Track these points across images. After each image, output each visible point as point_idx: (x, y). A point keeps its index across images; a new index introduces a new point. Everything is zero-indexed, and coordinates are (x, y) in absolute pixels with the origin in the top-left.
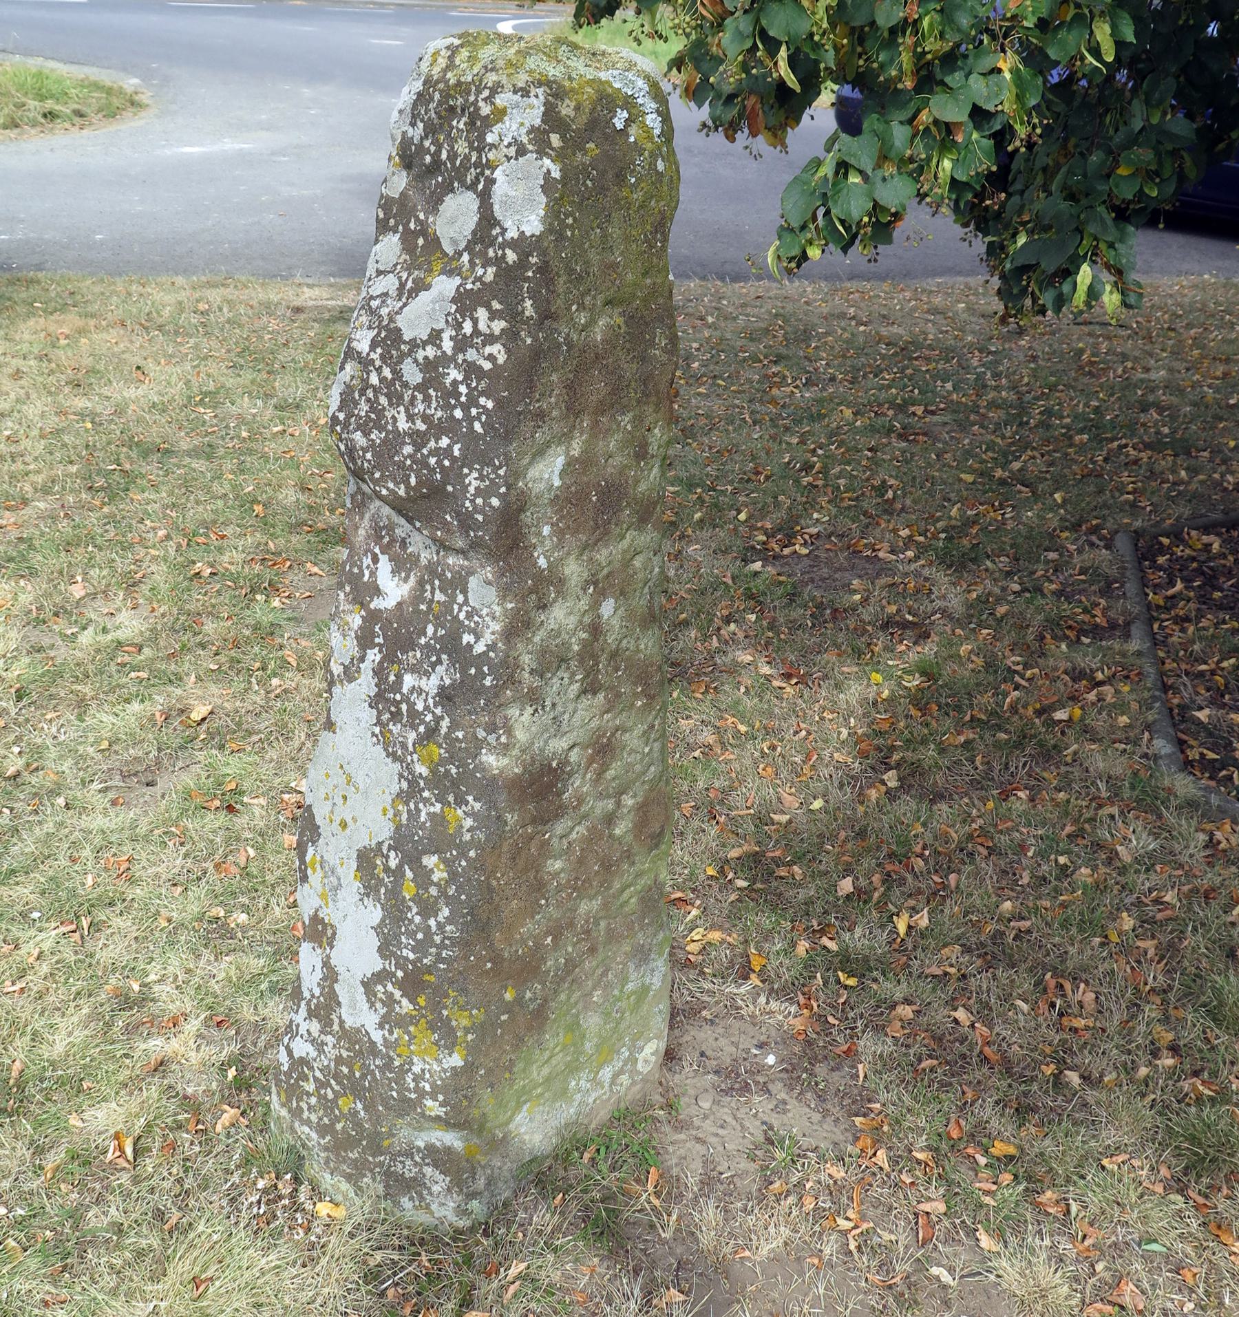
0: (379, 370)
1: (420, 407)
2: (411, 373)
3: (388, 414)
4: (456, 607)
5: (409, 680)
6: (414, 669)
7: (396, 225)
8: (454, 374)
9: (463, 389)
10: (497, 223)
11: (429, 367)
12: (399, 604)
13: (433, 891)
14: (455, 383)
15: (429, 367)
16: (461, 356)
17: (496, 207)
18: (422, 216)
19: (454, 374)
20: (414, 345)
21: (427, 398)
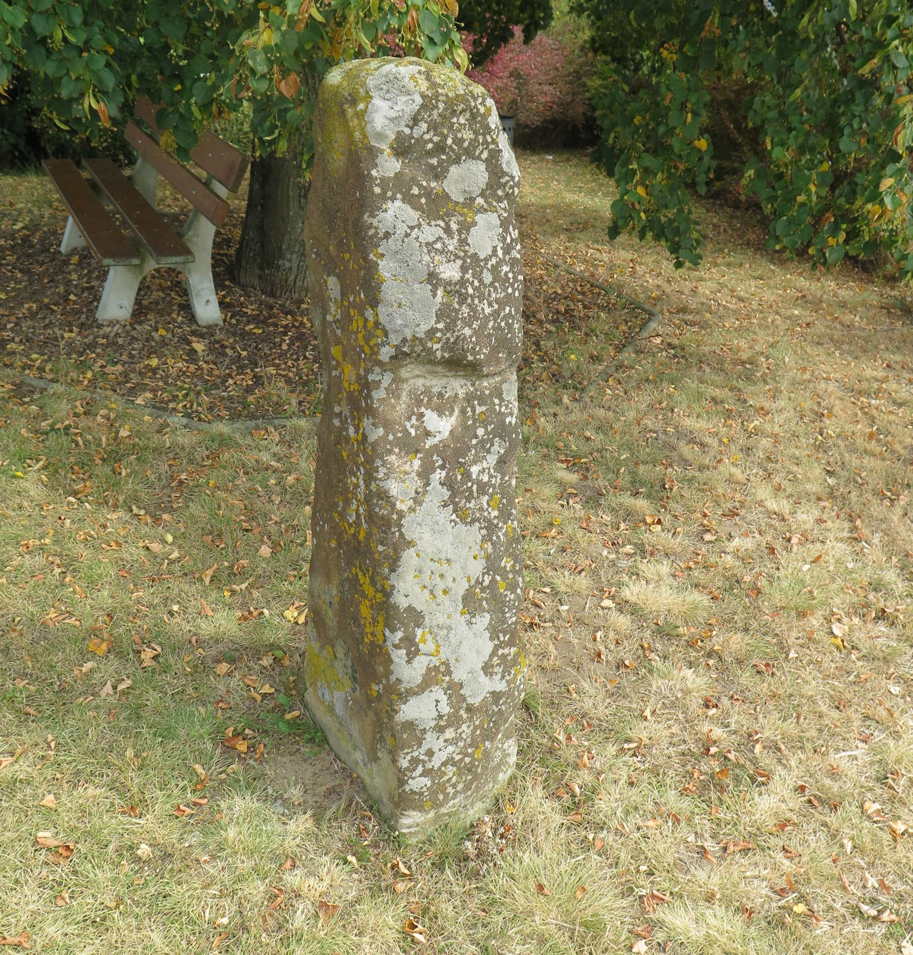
0: (472, 284)
1: (493, 295)
2: (488, 278)
3: (479, 308)
4: (497, 407)
5: (475, 470)
6: (475, 462)
7: (394, 195)
8: (506, 268)
9: (510, 275)
10: (504, 174)
11: (495, 270)
12: (451, 432)
13: (511, 576)
14: (506, 273)
15: (495, 270)
16: (507, 257)
17: (504, 166)
18: (425, 184)
19: (506, 268)
20: (486, 260)
21: (495, 289)
